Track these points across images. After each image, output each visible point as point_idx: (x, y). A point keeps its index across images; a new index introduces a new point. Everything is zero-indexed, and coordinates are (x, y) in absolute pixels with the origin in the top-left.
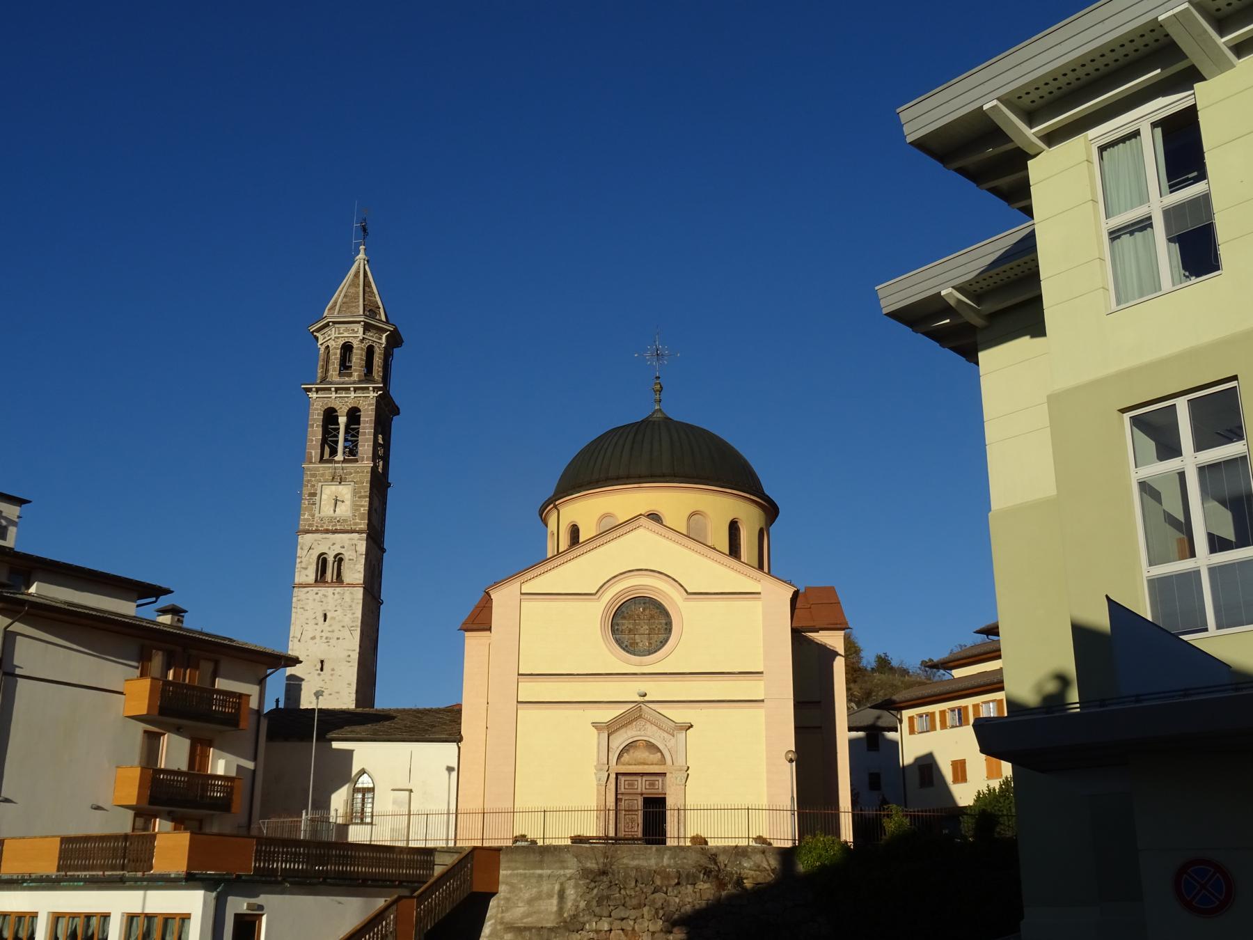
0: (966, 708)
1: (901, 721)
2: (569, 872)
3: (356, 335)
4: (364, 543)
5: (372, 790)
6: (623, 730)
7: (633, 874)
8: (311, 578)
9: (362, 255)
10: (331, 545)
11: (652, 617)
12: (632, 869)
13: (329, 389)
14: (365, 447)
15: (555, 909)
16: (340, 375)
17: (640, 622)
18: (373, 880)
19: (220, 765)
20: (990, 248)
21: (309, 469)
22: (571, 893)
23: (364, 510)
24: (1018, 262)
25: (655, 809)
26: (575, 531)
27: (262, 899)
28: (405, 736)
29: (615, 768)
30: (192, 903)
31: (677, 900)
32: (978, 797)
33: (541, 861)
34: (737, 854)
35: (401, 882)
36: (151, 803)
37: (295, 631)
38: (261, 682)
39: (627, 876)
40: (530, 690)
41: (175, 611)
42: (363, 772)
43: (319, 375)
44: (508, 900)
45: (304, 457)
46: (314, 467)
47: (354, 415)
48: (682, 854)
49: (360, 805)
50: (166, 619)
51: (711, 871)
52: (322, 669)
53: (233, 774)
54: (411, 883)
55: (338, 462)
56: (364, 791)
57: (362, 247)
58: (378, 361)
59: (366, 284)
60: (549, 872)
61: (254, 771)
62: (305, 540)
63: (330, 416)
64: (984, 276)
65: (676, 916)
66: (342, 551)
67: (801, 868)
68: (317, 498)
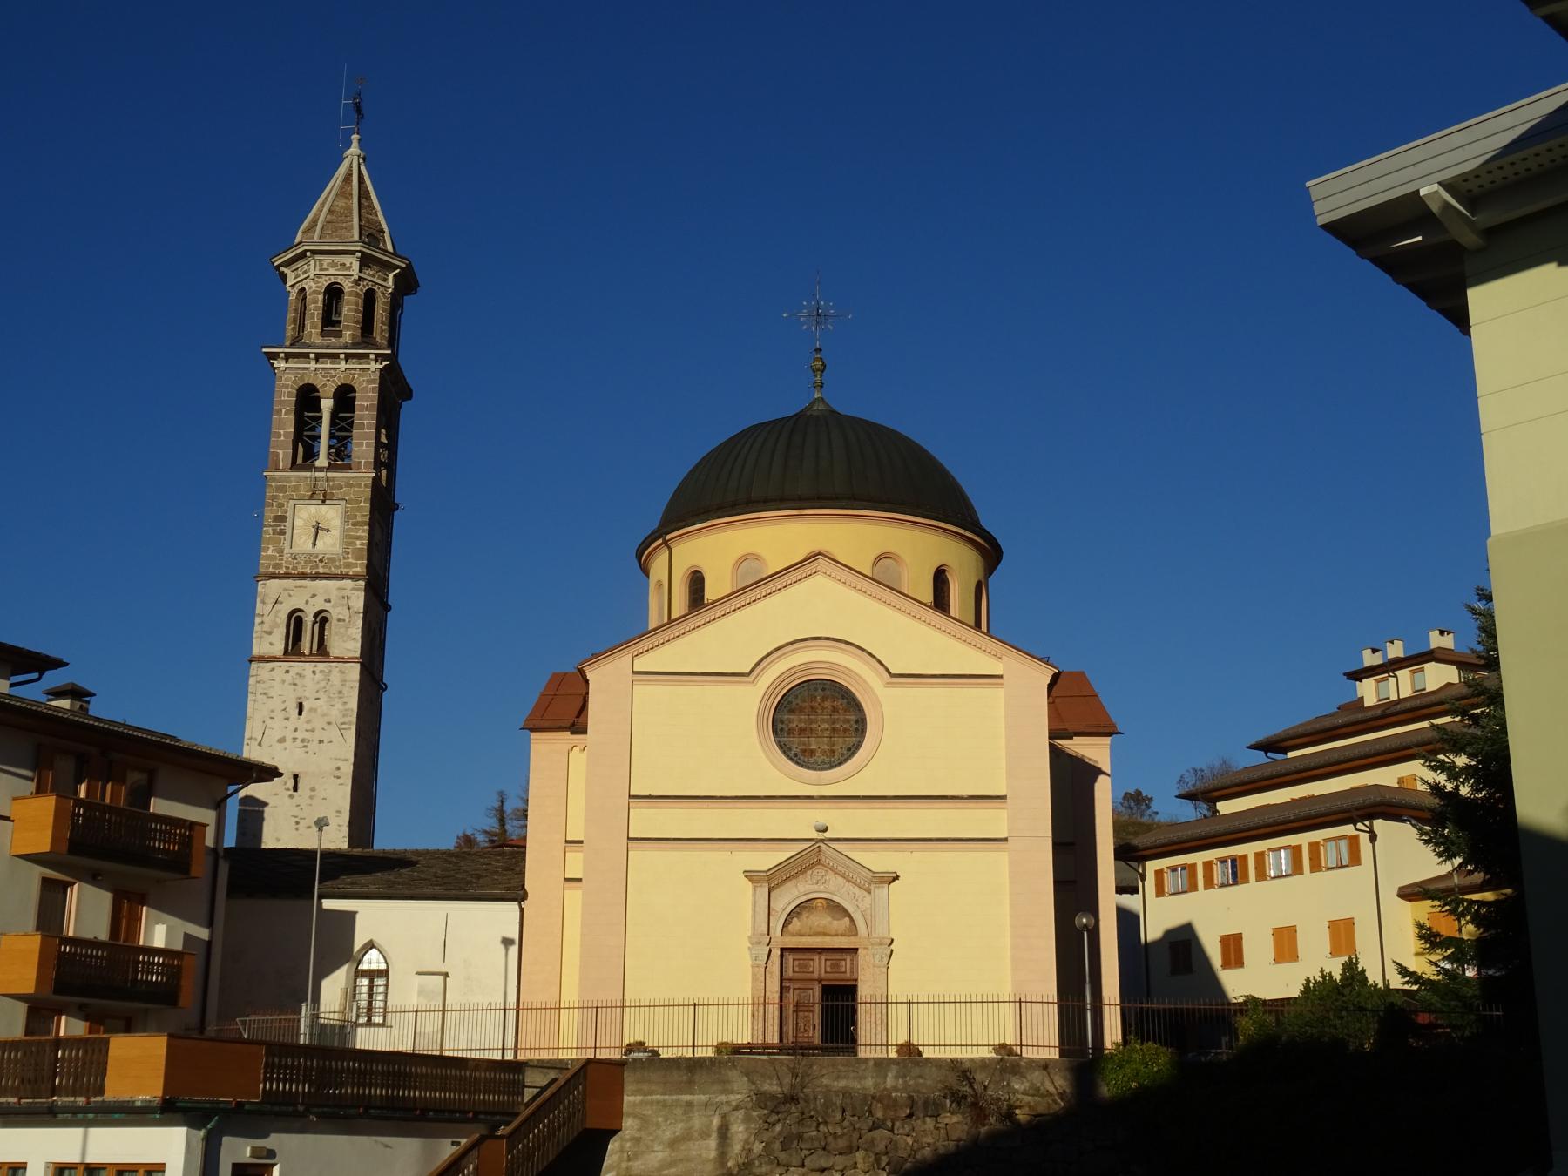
0: (1245, 857)
1: (1143, 878)
2: (735, 1098)
3: (348, 272)
4: (362, 595)
5: (384, 974)
6: (790, 884)
7: (839, 1101)
8: (278, 648)
9: (354, 149)
10: (309, 597)
11: (835, 710)
12: (837, 1093)
13: (306, 356)
14: (363, 446)
15: (713, 1154)
16: (323, 334)
17: (817, 718)
18: (436, 1111)
19: (158, 933)
20: (1507, 121)
21: (274, 479)
22: (738, 1130)
23: (361, 544)
24: (1533, 150)
25: (842, 1005)
26: (697, 582)
27: (273, 1141)
28: (439, 890)
29: (780, 941)
30: (170, 1144)
31: (910, 1140)
32: (1307, 986)
33: (691, 1082)
34: (1003, 1070)
35: (476, 1113)
36: (56, 992)
37: (252, 729)
38: (219, 805)
39: (828, 1104)
40: (647, 821)
41: (76, 693)
42: (370, 945)
43: (289, 333)
44: (637, 1141)
45: (265, 460)
46: (283, 477)
47: (345, 397)
48: (917, 1071)
49: (365, 996)
50: (65, 704)
51: (964, 1097)
52: (295, 789)
53: (178, 945)
54: (489, 1117)
55: (321, 469)
56: (372, 975)
57: (355, 137)
58: (381, 313)
59: (363, 194)
60: (704, 1098)
61: (209, 943)
62: (269, 588)
63: (307, 398)
64: (1492, 166)
65: (908, 1165)
66: (327, 606)
67: (1105, 1091)
68: (288, 524)
